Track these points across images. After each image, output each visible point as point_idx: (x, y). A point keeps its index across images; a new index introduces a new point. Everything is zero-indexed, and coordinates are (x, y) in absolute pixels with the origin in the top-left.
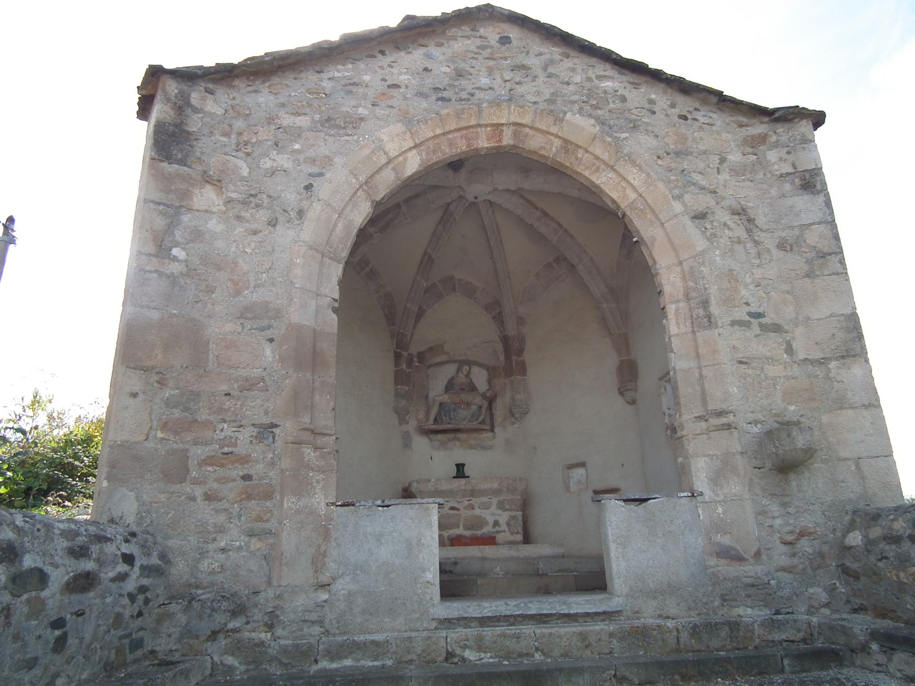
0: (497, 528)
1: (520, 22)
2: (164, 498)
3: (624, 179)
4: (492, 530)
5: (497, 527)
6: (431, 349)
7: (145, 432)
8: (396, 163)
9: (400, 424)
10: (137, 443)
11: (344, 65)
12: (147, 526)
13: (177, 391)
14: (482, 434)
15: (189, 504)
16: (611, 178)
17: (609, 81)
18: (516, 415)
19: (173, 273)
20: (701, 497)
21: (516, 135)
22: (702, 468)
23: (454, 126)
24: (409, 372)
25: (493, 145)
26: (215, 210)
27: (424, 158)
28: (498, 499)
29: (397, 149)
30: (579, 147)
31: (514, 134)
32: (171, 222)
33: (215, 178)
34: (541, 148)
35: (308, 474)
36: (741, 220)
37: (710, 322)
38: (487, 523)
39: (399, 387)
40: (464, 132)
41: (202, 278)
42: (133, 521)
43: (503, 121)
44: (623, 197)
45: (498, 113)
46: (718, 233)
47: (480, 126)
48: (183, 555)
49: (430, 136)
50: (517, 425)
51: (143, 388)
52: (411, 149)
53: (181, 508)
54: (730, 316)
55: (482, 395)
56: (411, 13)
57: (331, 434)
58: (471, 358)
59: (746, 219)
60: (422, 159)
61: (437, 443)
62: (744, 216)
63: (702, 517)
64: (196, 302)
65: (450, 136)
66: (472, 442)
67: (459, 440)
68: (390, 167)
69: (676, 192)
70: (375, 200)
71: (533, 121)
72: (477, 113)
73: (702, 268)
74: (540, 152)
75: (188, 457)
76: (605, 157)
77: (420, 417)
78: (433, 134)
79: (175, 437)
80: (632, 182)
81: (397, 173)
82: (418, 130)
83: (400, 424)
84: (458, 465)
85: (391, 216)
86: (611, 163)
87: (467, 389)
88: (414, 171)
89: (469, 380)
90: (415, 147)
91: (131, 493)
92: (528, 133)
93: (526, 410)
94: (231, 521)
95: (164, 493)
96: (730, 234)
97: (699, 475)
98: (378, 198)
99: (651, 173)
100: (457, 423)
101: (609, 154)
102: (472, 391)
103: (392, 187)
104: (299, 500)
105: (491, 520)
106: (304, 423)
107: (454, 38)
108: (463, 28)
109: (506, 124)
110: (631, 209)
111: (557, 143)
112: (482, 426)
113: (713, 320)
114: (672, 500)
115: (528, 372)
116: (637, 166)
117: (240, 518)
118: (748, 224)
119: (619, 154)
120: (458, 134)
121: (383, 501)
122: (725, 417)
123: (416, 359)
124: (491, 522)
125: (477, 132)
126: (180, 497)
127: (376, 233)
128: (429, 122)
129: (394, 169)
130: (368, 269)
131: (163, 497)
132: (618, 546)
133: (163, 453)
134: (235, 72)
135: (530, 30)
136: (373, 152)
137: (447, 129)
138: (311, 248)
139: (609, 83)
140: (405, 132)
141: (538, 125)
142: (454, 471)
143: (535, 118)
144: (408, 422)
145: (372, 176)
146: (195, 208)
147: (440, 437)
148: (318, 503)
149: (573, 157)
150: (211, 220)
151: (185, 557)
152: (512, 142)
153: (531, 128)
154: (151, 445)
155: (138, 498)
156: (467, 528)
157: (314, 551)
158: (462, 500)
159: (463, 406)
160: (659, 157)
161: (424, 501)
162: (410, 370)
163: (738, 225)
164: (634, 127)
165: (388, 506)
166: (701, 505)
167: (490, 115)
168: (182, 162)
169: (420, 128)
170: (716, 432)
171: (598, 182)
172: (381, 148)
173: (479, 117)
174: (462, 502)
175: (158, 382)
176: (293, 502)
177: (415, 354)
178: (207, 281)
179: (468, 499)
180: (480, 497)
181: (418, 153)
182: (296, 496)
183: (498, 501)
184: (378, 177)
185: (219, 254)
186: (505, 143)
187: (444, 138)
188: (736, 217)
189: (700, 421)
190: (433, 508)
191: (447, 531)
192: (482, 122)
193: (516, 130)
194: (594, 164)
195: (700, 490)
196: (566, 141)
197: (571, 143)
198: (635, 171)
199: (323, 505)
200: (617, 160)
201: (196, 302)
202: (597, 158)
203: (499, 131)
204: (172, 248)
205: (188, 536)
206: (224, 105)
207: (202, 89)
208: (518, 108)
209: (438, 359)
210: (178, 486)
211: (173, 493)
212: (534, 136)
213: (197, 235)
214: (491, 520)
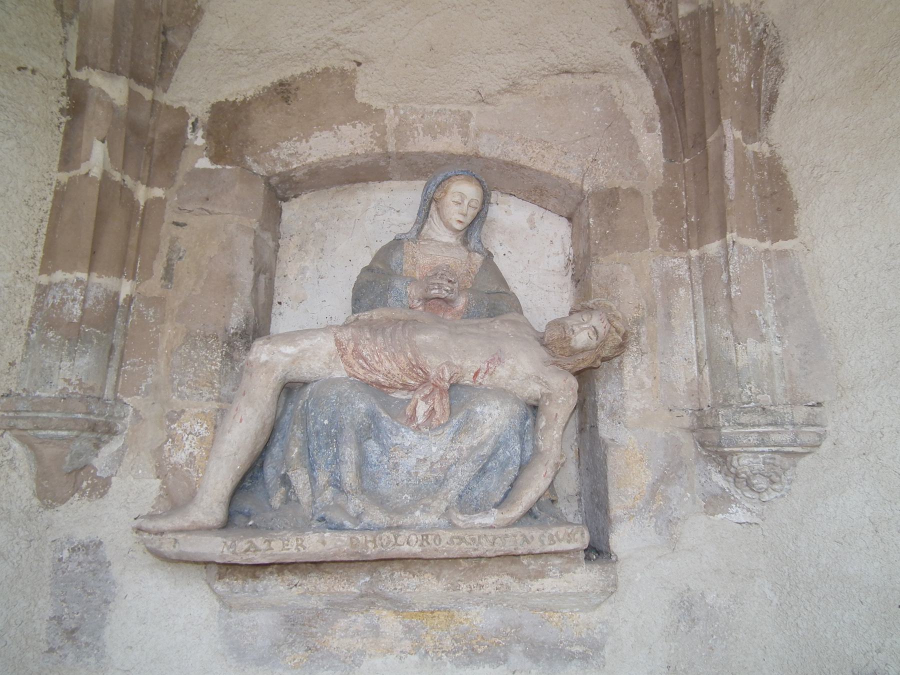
18: (744, 462)
24: (160, 202)
39: (59, 276)
50: (737, 514)
55: (542, 341)
58: (489, 148)
67: (398, 606)
77: (180, 457)
87: (461, 303)
89: (478, 258)
93: (808, 435)
100: (377, 516)
102: (494, 312)
115: (802, 218)
123: (199, 139)
144: (101, 487)
159: (422, 409)
162: (158, 192)
170: (307, 328)
177: (199, 110)
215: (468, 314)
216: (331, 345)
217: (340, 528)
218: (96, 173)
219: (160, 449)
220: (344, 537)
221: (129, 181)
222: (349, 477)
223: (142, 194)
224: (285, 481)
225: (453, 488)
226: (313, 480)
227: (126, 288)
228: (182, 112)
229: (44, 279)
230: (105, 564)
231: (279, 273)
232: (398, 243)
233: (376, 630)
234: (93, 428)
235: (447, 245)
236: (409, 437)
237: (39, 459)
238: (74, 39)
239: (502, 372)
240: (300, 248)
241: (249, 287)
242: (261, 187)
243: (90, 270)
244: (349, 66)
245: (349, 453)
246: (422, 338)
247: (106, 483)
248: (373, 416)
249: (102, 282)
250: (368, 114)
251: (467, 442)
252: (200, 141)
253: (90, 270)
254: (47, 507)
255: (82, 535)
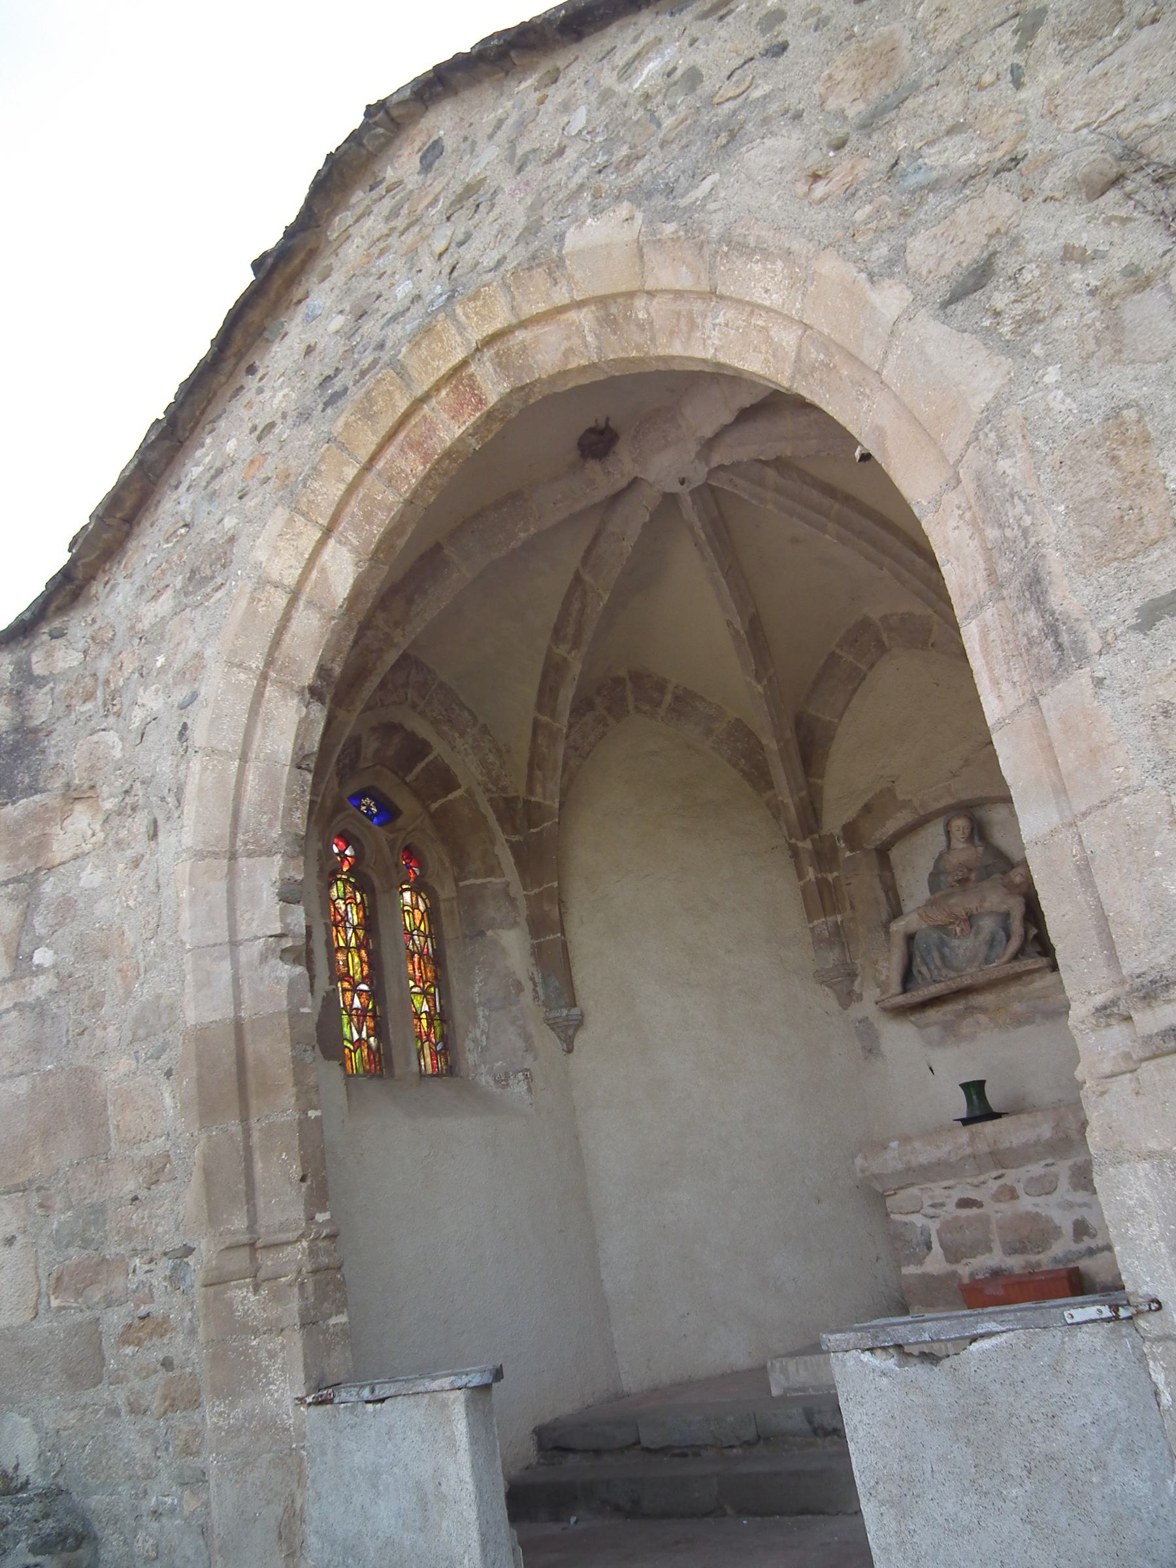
0: (1088, 1242)
1: (440, 89)
2: (73, 1418)
3: (755, 307)
4: (1075, 1247)
5: (1085, 1238)
6: (867, 809)
7: (31, 1304)
8: (308, 590)
9: (845, 1005)
10: (23, 1327)
11: (203, 445)
12: (56, 1475)
13: (69, 1213)
14: (1032, 982)
15: (111, 1423)
16: (727, 325)
17: (650, 60)
19: (38, 998)
20: (1153, 1317)
21: (503, 364)
22: (1143, 1203)
23: (371, 441)
24: (837, 878)
25: (473, 419)
26: (87, 848)
27: (355, 542)
28: (1070, 1162)
29: (293, 562)
30: (631, 295)
31: (500, 364)
32: (28, 906)
33: (86, 786)
34: (567, 354)
35: (247, 1345)
36: (1129, 196)
37: (1059, 646)
38: (1057, 1231)
39: (816, 922)
40: (401, 436)
41: (82, 986)
42: (33, 1470)
43: (459, 356)
44: (774, 356)
45: (436, 346)
46: (1044, 308)
47: (425, 398)
48: (116, 1523)
49: (340, 493)
51: (22, 1224)
52: (322, 543)
53: (101, 1434)
54: (1132, 591)
56: (256, 255)
57: (291, 1239)
59: (1147, 181)
60: (354, 550)
61: (934, 1031)
62: (1139, 177)
63: (1166, 1399)
64: (79, 1035)
65: (380, 465)
66: (1018, 1007)
67: (983, 1010)
68: (301, 604)
69: (882, 250)
70: (304, 688)
71: (513, 308)
72: (399, 380)
73: (1004, 464)
74: (570, 367)
75: (101, 1333)
76: (684, 279)
77: (883, 978)
78: (343, 487)
79: (76, 1301)
80: (767, 303)
81: (321, 607)
82: (312, 497)
83: (845, 1005)
84: (965, 1087)
85: (577, 605)
86: (705, 286)
87: (973, 876)
88: (351, 581)
90: (328, 532)
91: (25, 1420)
92: (523, 341)
94: (158, 1454)
95: (72, 1409)
96: (1092, 276)
97: (1132, 1231)
98: (308, 676)
99: (796, 246)
100: (953, 974)
101: (688, 266)
103: (324, 642)
104: (232, 1406)
105: (1065, 1221)
106: (234, 1233)
107: (346, 236)
108: (353, 200)
109: (472, 356)
110: (805, 376)
111: (585, 318)
112: (1018, 967)
113: (1065, 638)
114: (1046, 1338)
116: (754, 251)
117: (167, 1449)
118: (1161, 194)
119: (706, 251)
120: (391, 450)
121: (373, 1391)
122: (1169, 1002)
124: (1068, 1228)
125: (424, 417)
126: (97, 1411)
127: (569, 652)
128: (323, 468)
129: (310, 603)
130: (668, 698)
131: (71, 1418)
132: (883, 1509)
133: (62, 1335)
134: (79, 574)
135: (474, 82)
136: (252, 599)
137: (364, 455)
138: (200, 855)
139: (651, 65)
140: (291, 520)
141: (528, 311)
142: (959, 1105)
143: (513, 298)
144: (860, 997)
145: (276, 642)
146: (58, 861)
147: (933, 1014)
148: (277, 1401)
149: (633, 328)
150: (83, 869)
151: (118, 1526)
152: (505, 387)
153: (523, 324)
154: (42, 1325)
155: (36, 1427)
156: (1012, 1250)
157: (280, 1510)
158: (982, 1178)
159: (958, 930)
160: (816, 177)
161: (435, 1385)
162: (835, 874)
163: (1124, 221)
164: (732, 136)
165: (382, 1400)
166: (1158, 1349)
167: (426, 363)
168: (33, 789)
169: (313, 491)
171: (709, 354)
172: (264, 582)
173: (408, 385)
174: (983, 1183)
175: (41, 1206)
176: (220, 1414)
177: (837, 831)
178: (89, 987)
179: (995, 1174)
180: (1020, 1165)
181: (340, 542)
182: (225, 1398)
183: (1070, 1168)
184: (287, 638)
185: (101, 929)
186: (493, 399)
187: (370, 477)
188: (1113, 195)
189: (1108, 1025)
190: (453, 1403)
191: (964, 1261)
192: (419, 392)
193: (497, 354)
194: (679, 314)
195: (1145, 1290)
196: (602, 301)
197: (614, 297)
198: (757, 268)
199: (289, 1402)
200: (712, 269)
201: (79, 1035)
202: (679, 294)
203: (465, 381)
204: (33, 952)
205: (118, 1484)
206: (81, 645)
207: (46, 637)
208: (472, 304)
209: (891, 826)
210: (92, 1392)
211: (85, 1407)
212: (536, 339)
213: (66, 906)
214: (1065, 1221)
215: (980, 880)
216: (917, 916)
217: (941, 981)
218: (813, 879)
219: (875, 977)
220: (943, 984)
221: (825, 876)
222: (938, 962)
223: (830, 877)
224: (920, 972)
225: (981, 956)
226: (929, 969)
227: (839, 918)
228: (832, 836)
229: (811, 925)
230: (872, 1024)
231: (898, 886)
232: (941, 856)
233: (978, 1023)
234: (849, 975)
235: (962, 849)
236: (956, 942)
237: (835, 991)
238: (784, 828)
239: (987, 905)
240: (903, 870)
241: (885, 900)
242: (874, 854)
243: (825, 916)
244: (890, 785)
245: (936, 954)
246: (952, 901)
247: (861, 995)
248: (941, 938)
249: (831, 919)
250: (906, 804)
251: (981, 937)
252: (843, 845)
253: (825, 916)
254: (845, 1009)
255: (860, 1016)
